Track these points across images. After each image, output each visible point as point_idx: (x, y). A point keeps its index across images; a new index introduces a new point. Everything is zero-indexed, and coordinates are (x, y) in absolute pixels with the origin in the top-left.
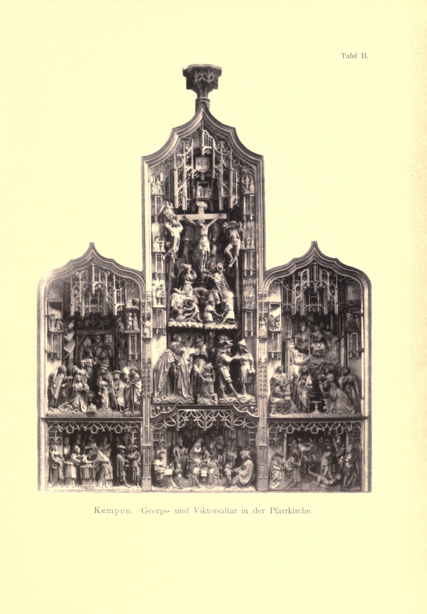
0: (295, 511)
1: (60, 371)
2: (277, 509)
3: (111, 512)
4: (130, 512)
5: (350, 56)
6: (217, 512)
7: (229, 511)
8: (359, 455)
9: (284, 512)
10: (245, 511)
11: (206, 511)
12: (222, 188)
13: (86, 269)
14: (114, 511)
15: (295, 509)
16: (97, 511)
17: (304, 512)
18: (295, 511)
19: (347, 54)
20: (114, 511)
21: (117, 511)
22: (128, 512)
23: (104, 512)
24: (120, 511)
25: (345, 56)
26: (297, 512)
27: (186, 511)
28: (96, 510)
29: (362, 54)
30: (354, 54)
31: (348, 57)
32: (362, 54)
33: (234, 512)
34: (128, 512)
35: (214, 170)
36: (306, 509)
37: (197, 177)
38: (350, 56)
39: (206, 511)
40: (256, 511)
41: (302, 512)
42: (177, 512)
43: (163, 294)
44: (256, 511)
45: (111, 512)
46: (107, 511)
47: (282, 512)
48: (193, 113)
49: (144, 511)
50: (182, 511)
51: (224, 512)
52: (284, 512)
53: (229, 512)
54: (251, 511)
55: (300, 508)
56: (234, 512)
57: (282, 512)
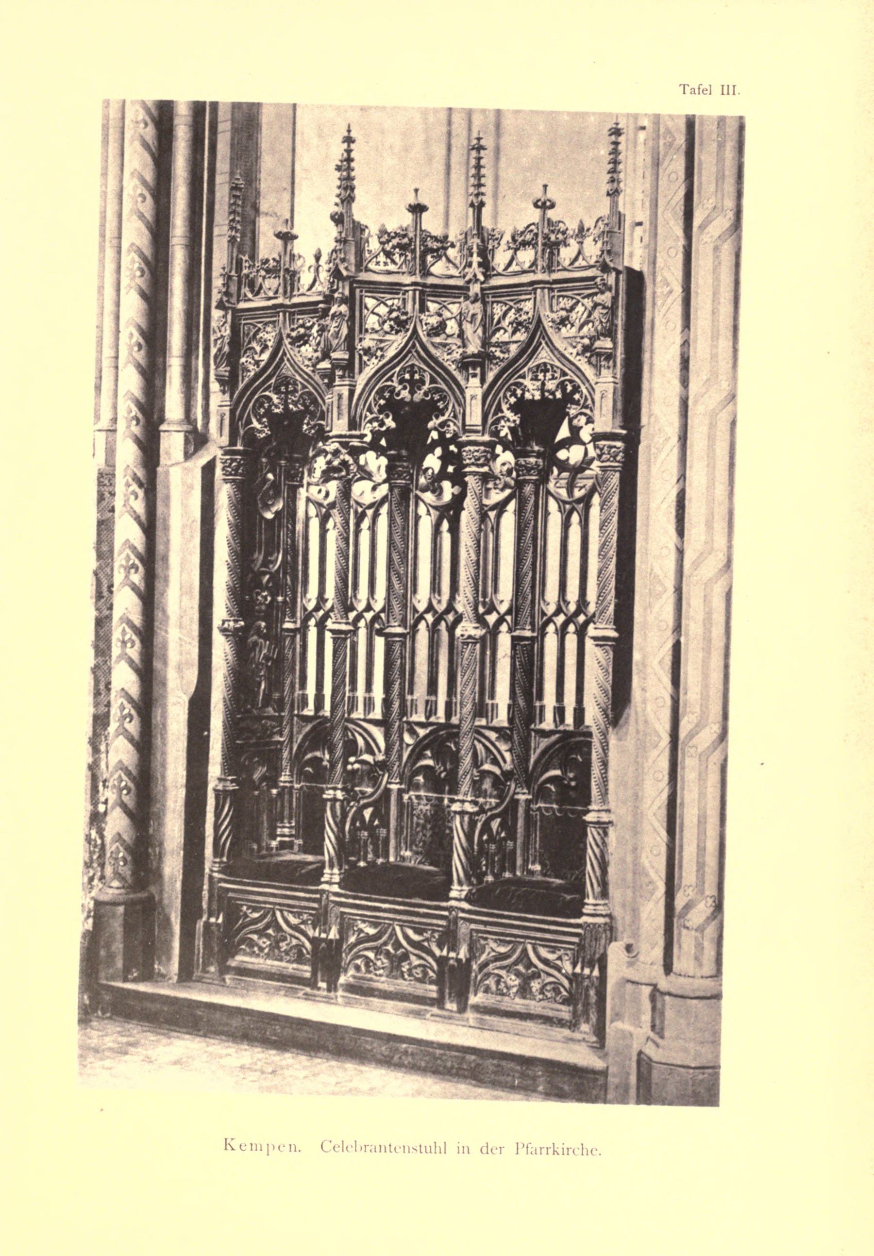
0: (566, 1151)
2: (530, 1146)
3: (259, 1148)
5: (697, 91)
8: (406, 1067)
13: (367, 270)
14: (265, 1148)
15: (565, 1147)
16: (228, 1147)
18: (566, 1151)
19: (691, 87)
20: (265, 1148)
21: (271, 1147)
22: (293, 1148)
23: (243, 1148)
24: (276, 1147)
25: (688, 89)
26: (571, 1151)
28: (227, 1145)
29: (723, 86)
30: (705, 86)
31: (693, 91)
32: (723, 86)
34: (293, 1148)
36: (588, 1146)
38: (697, 91)
40: (487, 1150)
42: (466, 1149)
43: (617, 381)
44: (487, 1150)
45: (259, 1148)
46: (249, 1147)
47: (538, 1151)
48: (357, 218)
52: (544, 1151)
54: (475, 1150)
55: (574, 1144)
57: (538, 1151)
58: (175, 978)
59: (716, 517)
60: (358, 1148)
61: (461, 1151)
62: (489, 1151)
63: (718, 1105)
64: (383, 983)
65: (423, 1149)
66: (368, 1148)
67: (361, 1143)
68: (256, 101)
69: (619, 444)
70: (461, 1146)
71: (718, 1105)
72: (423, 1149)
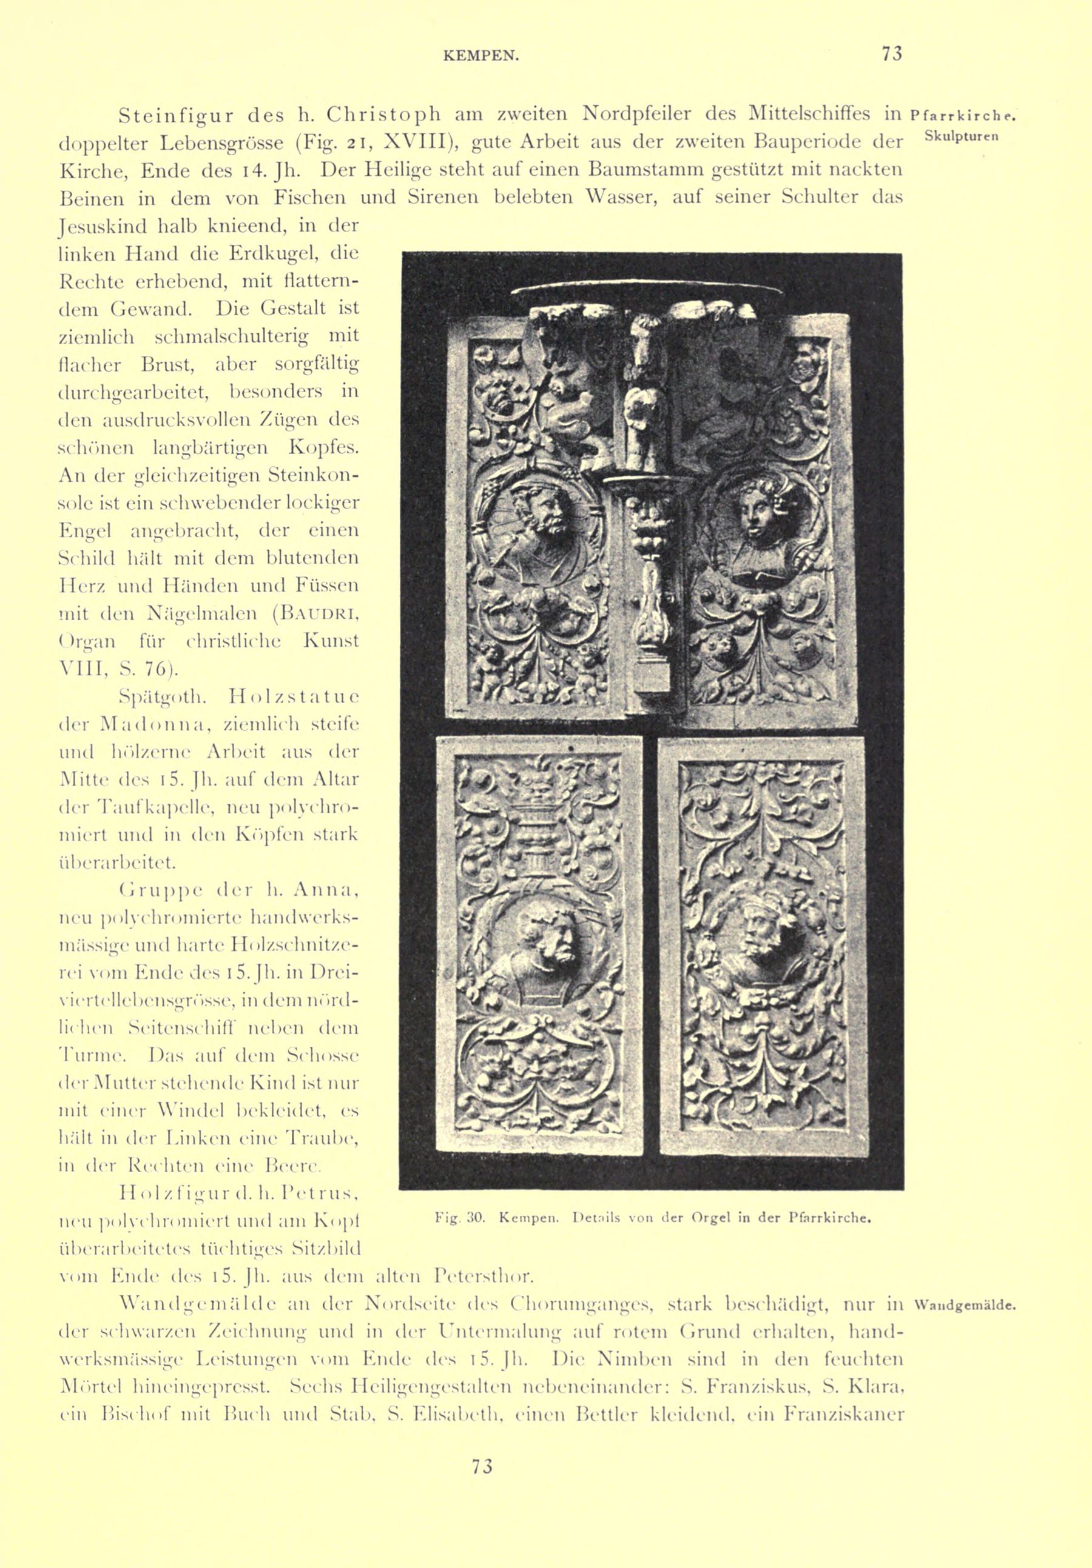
0: (426, 198)
1: (684, 453)
4: (278, 893)
6: (313, 392)
7: (340, 781)
9: (816, 1219)
10: (746, 1219)
11: (873, 170)
12: (575, 306)
14: (162, 892)
16: (295, 449)
17: (107, 174)
20: (162, 892)
21: (184, 891)
22: (552, 1219)
24: (191, 892)
27: (734, 1333)
33: (351, 781)
34: (552, 1219)
35: (575, 306)
37: (754, 544)
39: (873, 170)
41: (803, 199)
42: (140, 948)
46: (191, 727)
49: (268, 308)
50: (877, 1332)
51: (794, 1334)
53: (339, 782)
56: (351, 781)
58: (716, 823)
59: (804, 984)
60: (181, 532)
61: (890, 116)
62: (262, 506)
63: (408, 258)
64: (480, 402)
65: (241, 1360)
66: (193, 532)
67: (658, 107)
68: (401, 257)
69: (457, 355)
70: (150, 1383)
71: (408, 258)
72: (241, 1360)
